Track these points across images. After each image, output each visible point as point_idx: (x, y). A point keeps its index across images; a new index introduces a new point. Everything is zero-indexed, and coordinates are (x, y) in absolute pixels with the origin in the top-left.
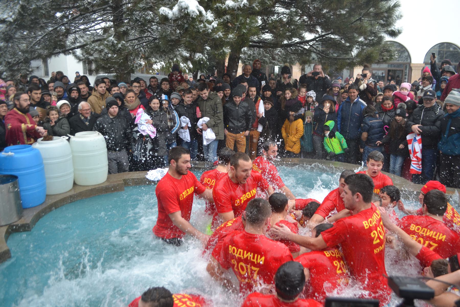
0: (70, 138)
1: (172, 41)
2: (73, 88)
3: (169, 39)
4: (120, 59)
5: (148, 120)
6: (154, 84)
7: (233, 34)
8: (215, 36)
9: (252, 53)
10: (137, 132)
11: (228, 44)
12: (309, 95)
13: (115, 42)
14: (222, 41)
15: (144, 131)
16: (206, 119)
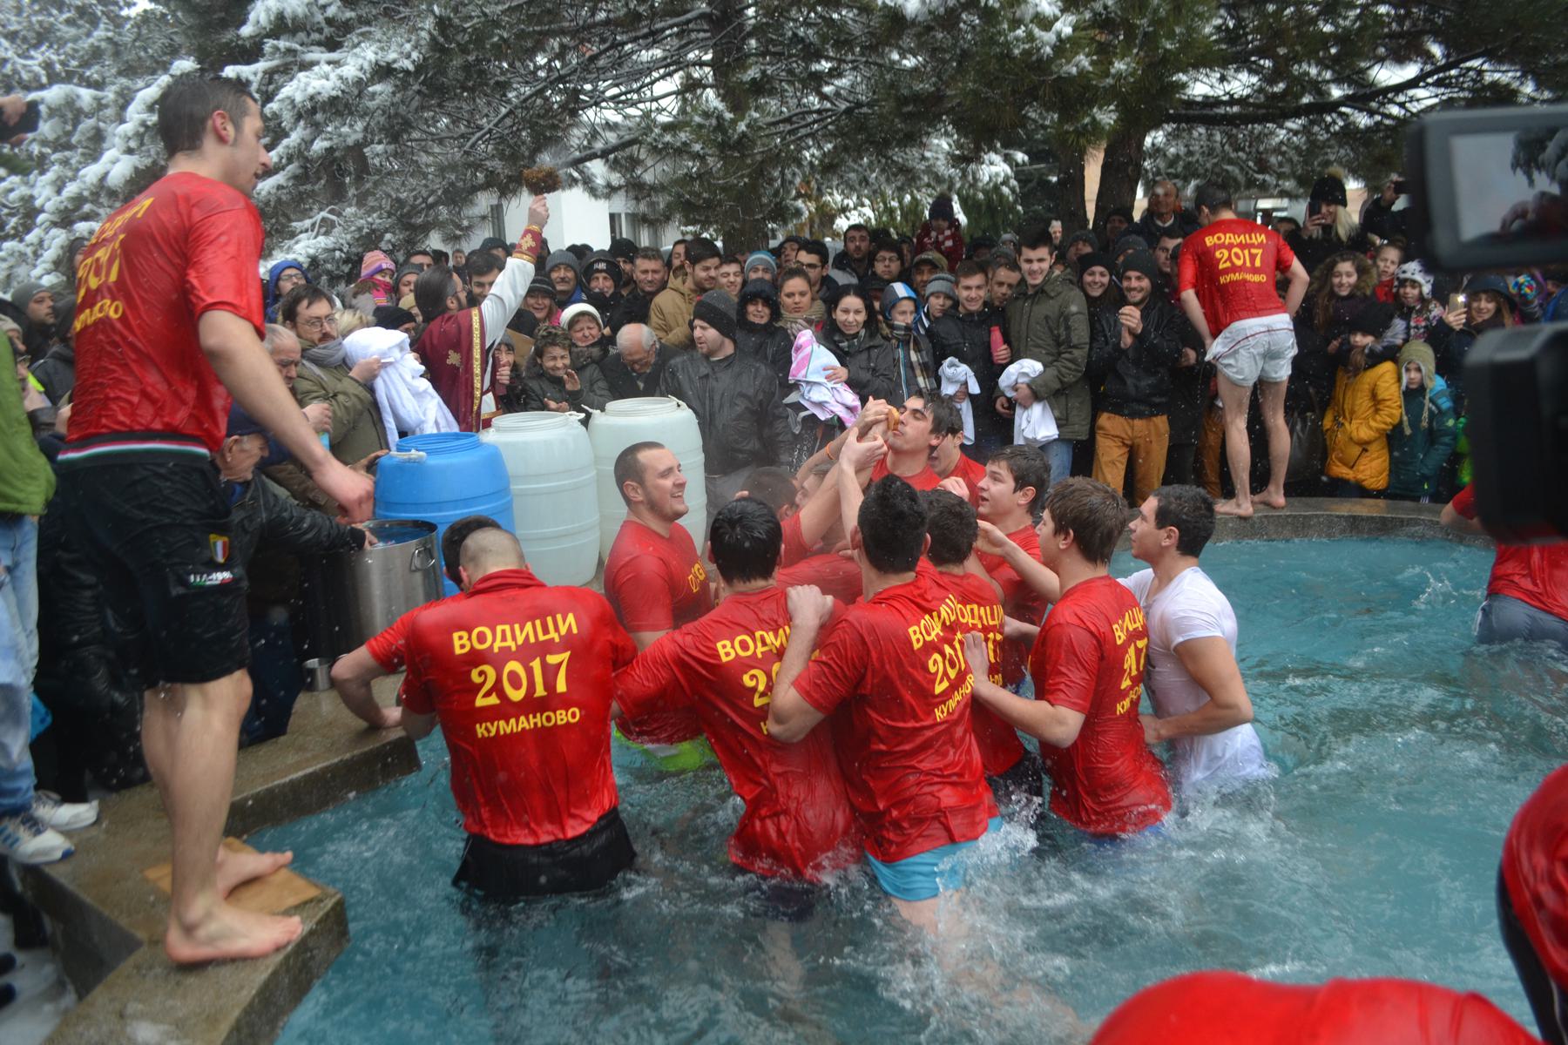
0: (589, 415)
1: (916, 98)
2: (596, 266)
3: (905, 92)
4: (742, 176)
5: (833, 368)
6: (858, 248)
7: (1128, 59)
8: (1065, 68)
9: (1183, 150)
10: (798, 407)
11: (1111, 95)
12: (1408, 275)
13: (729, 116)
14: (1087, 87)
15: (821, 405)
16: (1030, 367)
